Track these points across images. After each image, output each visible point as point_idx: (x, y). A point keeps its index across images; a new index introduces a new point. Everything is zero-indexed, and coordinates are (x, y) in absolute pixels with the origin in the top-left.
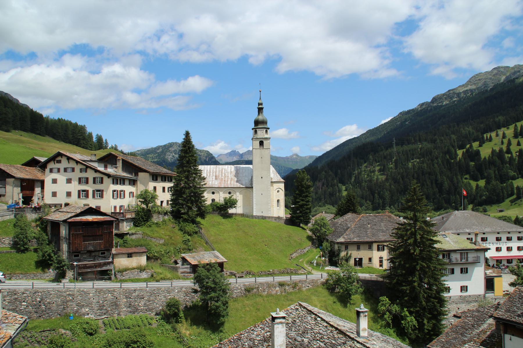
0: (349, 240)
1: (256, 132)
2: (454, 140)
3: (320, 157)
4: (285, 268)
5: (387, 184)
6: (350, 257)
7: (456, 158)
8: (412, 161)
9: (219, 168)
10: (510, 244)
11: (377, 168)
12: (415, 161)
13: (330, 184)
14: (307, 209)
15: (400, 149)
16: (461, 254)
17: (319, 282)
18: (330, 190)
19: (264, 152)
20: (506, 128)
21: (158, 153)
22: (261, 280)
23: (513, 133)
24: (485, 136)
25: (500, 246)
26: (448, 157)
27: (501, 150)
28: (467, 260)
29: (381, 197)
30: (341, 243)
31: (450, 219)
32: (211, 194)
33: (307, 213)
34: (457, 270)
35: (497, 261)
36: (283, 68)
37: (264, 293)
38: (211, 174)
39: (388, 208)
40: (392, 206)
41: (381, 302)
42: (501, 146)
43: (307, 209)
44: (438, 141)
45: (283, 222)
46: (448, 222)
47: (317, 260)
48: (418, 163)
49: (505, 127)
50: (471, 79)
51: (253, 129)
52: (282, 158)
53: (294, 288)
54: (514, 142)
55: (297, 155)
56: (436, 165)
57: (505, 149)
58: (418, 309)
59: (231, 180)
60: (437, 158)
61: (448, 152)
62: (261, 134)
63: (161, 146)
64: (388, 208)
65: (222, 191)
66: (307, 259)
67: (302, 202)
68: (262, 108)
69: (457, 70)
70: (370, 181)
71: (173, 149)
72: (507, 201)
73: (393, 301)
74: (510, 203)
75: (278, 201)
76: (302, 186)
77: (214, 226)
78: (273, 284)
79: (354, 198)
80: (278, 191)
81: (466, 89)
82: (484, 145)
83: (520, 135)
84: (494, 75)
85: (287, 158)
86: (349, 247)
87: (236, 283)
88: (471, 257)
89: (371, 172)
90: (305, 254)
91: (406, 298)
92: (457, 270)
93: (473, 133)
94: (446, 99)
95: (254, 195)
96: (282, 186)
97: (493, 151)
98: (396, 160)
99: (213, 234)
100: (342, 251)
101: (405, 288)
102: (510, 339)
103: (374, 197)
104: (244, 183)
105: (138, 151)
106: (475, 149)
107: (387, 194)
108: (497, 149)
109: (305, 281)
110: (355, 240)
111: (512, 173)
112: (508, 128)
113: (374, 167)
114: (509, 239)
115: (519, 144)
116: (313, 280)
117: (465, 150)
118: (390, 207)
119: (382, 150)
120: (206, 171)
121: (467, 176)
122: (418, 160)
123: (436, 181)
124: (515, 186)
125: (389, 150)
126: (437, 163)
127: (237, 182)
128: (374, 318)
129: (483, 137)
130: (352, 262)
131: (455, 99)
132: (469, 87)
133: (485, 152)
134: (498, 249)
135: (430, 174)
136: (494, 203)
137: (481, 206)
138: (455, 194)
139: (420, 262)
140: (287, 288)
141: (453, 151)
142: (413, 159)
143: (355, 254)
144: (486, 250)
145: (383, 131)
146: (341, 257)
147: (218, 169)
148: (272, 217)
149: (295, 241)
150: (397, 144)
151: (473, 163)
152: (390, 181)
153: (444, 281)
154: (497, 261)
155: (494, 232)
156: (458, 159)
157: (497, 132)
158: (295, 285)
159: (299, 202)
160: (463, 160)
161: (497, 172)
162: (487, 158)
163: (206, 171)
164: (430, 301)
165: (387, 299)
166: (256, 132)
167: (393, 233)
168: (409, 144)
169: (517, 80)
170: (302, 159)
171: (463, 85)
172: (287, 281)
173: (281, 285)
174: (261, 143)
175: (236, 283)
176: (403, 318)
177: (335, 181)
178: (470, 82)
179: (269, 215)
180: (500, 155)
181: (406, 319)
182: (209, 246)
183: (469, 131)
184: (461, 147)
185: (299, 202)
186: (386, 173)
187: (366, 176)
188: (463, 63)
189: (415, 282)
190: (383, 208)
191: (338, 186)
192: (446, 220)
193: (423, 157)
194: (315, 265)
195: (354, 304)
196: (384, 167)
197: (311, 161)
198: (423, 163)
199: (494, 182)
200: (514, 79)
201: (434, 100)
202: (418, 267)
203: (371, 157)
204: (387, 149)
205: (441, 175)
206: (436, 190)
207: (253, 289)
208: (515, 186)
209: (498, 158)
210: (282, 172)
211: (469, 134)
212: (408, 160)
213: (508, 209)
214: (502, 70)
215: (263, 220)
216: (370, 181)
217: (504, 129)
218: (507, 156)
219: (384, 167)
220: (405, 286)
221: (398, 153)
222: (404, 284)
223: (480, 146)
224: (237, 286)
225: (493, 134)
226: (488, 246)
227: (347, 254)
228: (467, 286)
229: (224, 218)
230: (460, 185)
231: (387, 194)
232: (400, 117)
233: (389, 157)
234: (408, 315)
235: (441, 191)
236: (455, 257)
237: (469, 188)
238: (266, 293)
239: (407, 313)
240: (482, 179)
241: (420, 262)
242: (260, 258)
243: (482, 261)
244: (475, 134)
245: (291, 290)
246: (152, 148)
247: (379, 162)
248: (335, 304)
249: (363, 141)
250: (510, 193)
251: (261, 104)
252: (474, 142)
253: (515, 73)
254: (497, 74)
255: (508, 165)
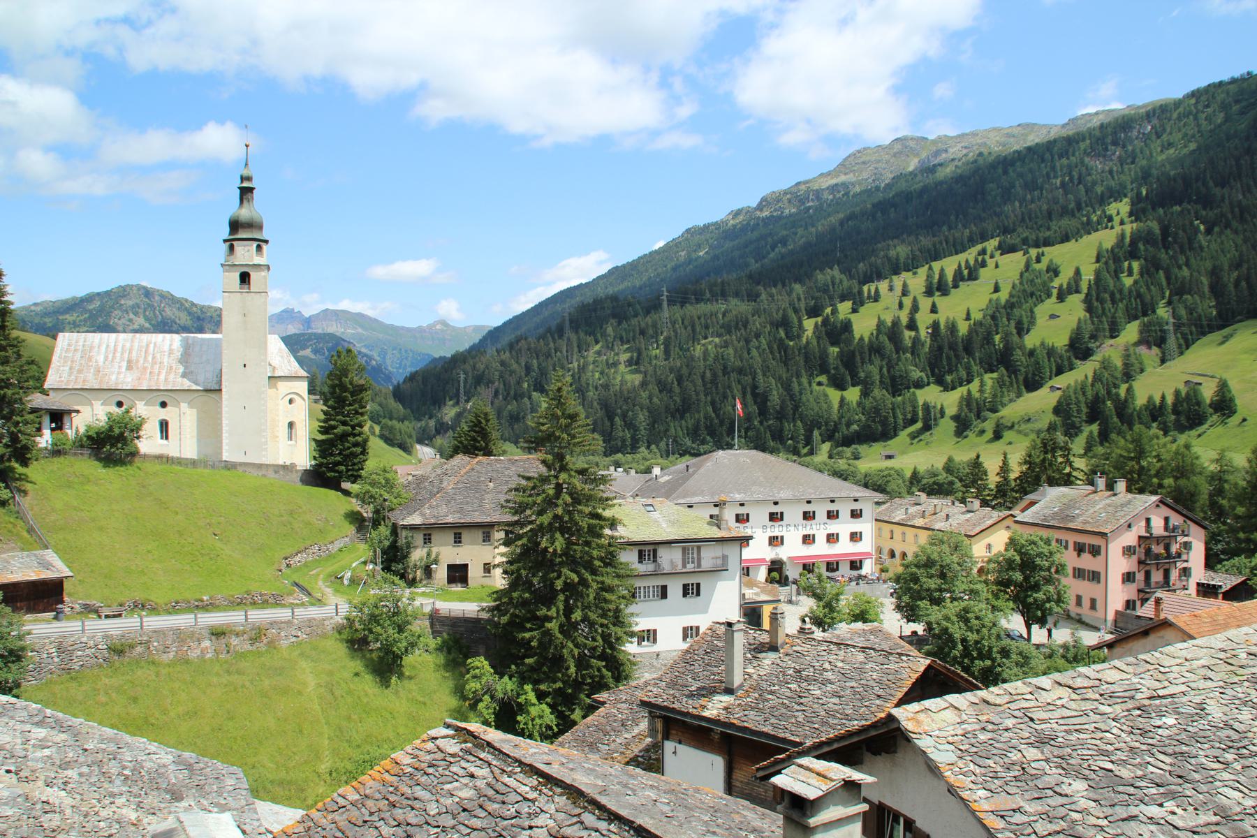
0: (433, 521)
1: (232, 248)
2: (798, 295)
3: (497, 329)
4: (248, 592)
5: (644, 395)
6: (436, 562)
7: (799, 337)
8: (703, 342)
9: (141, 341)
10: (833, 527)
11: (625, 357)
12: (710, 343)
13: (512, 393)
14: (356, 445)
15: (678, 312)
16: (684, 549)
17: (329, 626)
18: (512, 407)
19: (251, 300)
20: (910, 274)
21: (90, 311)
22: (155, 622)
23: (924, 284)
24: (865, 288)
25: (811, 532)
26: (782, 333)
27: (896, 323)
28: (699, 565)
29: (630, 425)
30: (413, 528)
31: (702, 470)
32: (158, 408)
33: (354, 455)
34: (675, 589)
35: (805, 566)
36: (434, 110)
37: (165, 656)
38: (118, 355)
39: (643, 449)
40: (653, 446)
41: (472, 672)
42: (898, 313)
43: (356, 445)
44: (763, 296)
45: (296, 477)
46: (696, 476)
47: (354, 570)
48: (716, 346)
49: (909, 270)
50: (845, 160)
51: (225, 241)
52: (409, 330)
53: (254, 640)
54: (925, 303)
55: (444, 323)
56: (754, 352)
57: (904, 320)
58: (559, 685)
59: (168, 373)
60: (757, 336)
61: (784, 323)
62: (245, 254)
63: (98, 294)
64: (643, 449)
65: (142, 400)
66: (330, 569)
67: (341, 429)
68: (251, 190)
69: (831, 140)
70: (606, 387)
71: (130, 303)
72: (904, 435)
73: (500, 670)
74: (908, 440)
75: (291, 425)
76: (343, 388)
77: (69, 485)
78: (193, 633)
79: (488, 421)
80: (291, 401)
81: (834, 181)
82: (862, 309)
83: (938, 289)
84: (894, 155)
85: (421, 330)
86: (463, 536)
87: (83, 630)
88: (709, 557)
89: (609, 366)
90: (330, 556)
91: (529, 661)
92: (675, 589)
93: (841, 281)
94: (789, 201)
95: (225, 409)
96: (303, 387)
97: (880, 324)
98: (667, 340)
99: (59, 505)
100: (415, 547)
101: (527, 635)
102: (675, 753)
103: (612, 425)
104: (201, 378)
105: (35, 304)
106: (841, 316)
107: (642, 418)
108: (889, 320)
109: (289, 623)
110: (450, 519)
111: (916, 374)
112: (915, 274)
113: (617, 354)
114: (832, 515)
115: (934, 310)
116: (310, 620)
117: (820, 319)
118: (648, 447)
119: (636, 316)
120: (103, 349)
121: (823, 378)
122: (717, 340)
123: (755, 387)
124: (921, 403)
125: (654, 316)
126: (758, 348)
127: (184, 375)
128: (459, 712)
129: (860, 292)
130: (441, 573)
131: (811, 204)
132: (842, 178)
133: (864, 325)
134: (808, 539)
135: (740, 371)
136: (875, 440)
137: (848, 445)
138: (794, 420)
139: (565, 570)
140: (234, 641)
141: (796, 320)
142: (706, 338)
143: (448, 554)
144: (745, 541)
145: (647, 271)
146: (411, 564)
147: (136, 344)
148: (267, 465)
149: (308, 524)
150: (671, 302)
151: (837, 350)
152: (650, 387)
153: (632, 614)
154: (805, 566)
155: (799, 500)
156: (804, 340)
157: (891, 281)
158: (257, 634)
159: (334, 427)
160: (815, 342)
161: (885, 370)
162: (866, 340)
163: (103, 349)
164: (589, 666)
165: (486, 663)
166: (232, 248)
167: (508, 501)
168: (698, 301)
169: (940, 169)
170: (458, 332)
171: (829, 174)
172: (235, 625)
173: (217, 633)
174: (245, 278)
175: (83, 630)
176: (522, 709)
177: (526, 385)
178: (843, 167)
179: (264, 461)
180: (893, 332)
181: (528, 713)
182: (36, 539)
183: (833, 278)
184: (814, 312)
185: (334, 427)
186: (642, 369)
187: (597, 375)
188: (844, 126)
189: (549, 619)
190: (634, 449)
191: (530, 398)
192: (694, 472)
193: (729, 332)
194: (346, 582)
195: (410, 678)
196: (639, 354)
197: (476, 339)
198: (726, 347)
199: (877, 392)
200: (935, 166)
201: (764, 203)
202: (559, 584)
203: (610, 330)
204: (648, 312)
205: (764, 375)
206: (754, 409)
207: (132, 647)
208: (921, 403)
209: (890, 339)
210: (408, 364)
211: (833, 283)
212: (694, 339)
213: (903, 453)
214: (912, 144)
215: (227, 473)
216: (606, 387)
217: (906, 275)
218: (908, 335)
219: (639, 354)
220: (531, 630)
221: (674, 323)
222: (528, 625)
223: (854, 311)
224: (84, 639)
225: (883, 286)
226: (748, 532)
227: (429, 554)
228: (655, 631)
229: (104, 467)
230: (804, 398)
231: (642, 418)
232: (687, 239)
233: (651, 332)
234: (534, 700)
235: (763, 412)
236: (670, 558)
237: (825, 406)
238: (171, 655)
239: (532, 697)
240: (853, 385)
241: (565, 570)
242: (188, 567)
243: (734, 567)
244: (846, 284)
245: (248, 647)
246: (74, 298)
247: (628, 342)
248: (357, 679)
249: (601, 292)
250: (909, 416)
251: (249, 179)
252: (842, 301)
253: (937, 153)
254: (900, 153)
255: (909, 355)
